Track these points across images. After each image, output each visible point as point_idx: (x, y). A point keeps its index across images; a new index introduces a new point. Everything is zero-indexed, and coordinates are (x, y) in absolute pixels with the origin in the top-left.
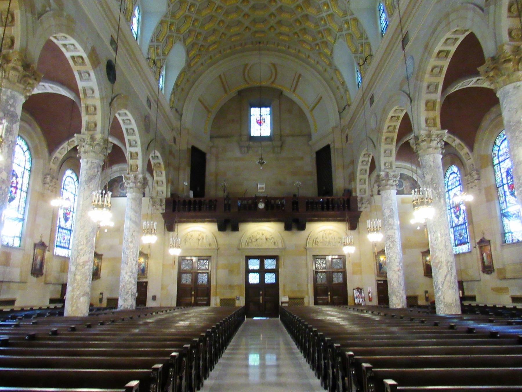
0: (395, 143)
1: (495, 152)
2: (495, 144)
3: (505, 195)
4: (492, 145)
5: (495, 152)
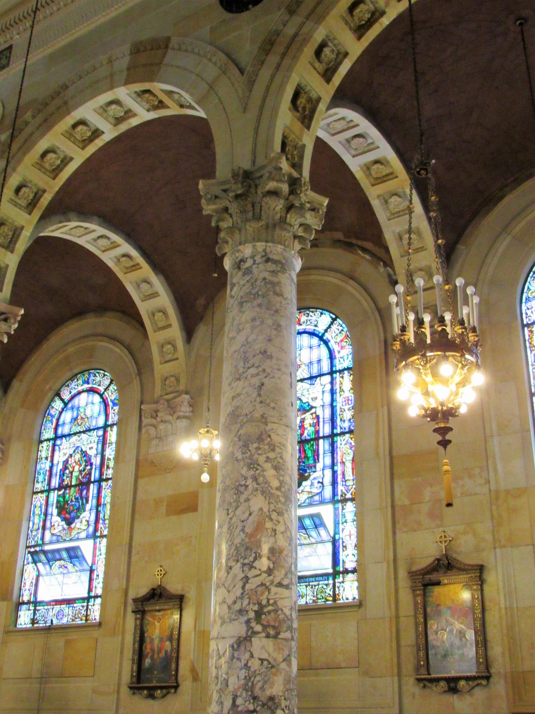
0: (37, 213)
1: (53, 412)
2: (58, 394)
3: (46, 514)
4: (50, 394)
5: (53, 412)
